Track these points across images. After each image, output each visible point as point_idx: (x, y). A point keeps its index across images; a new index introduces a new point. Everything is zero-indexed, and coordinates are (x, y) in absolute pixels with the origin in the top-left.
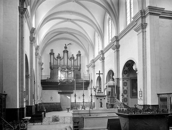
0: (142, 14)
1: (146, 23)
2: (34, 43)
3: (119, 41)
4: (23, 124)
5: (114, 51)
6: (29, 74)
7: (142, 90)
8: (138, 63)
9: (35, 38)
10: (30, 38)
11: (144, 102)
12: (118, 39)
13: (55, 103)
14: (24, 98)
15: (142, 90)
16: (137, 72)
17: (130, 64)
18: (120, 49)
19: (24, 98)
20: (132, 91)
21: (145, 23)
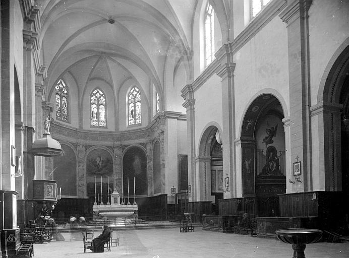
0: (227, 51)
1: (234, 62)
2: (35, 49)
3: (232, 55)
4: (12, 237)
5: (221, 79)
6: (22, 121)
7: (229, 176)
8: (222, 129)
9: (39, 10)
10: (23, 34)
11: (232, 195)
12: (192, 89)
13: (163, 144)
14: (13, 165)
15: (229, 176)
16: (222, 146)
17: (212, 131)
18: (235, 72)
19: (13, 165)
20: (342, 123)
21: (232, 63)
